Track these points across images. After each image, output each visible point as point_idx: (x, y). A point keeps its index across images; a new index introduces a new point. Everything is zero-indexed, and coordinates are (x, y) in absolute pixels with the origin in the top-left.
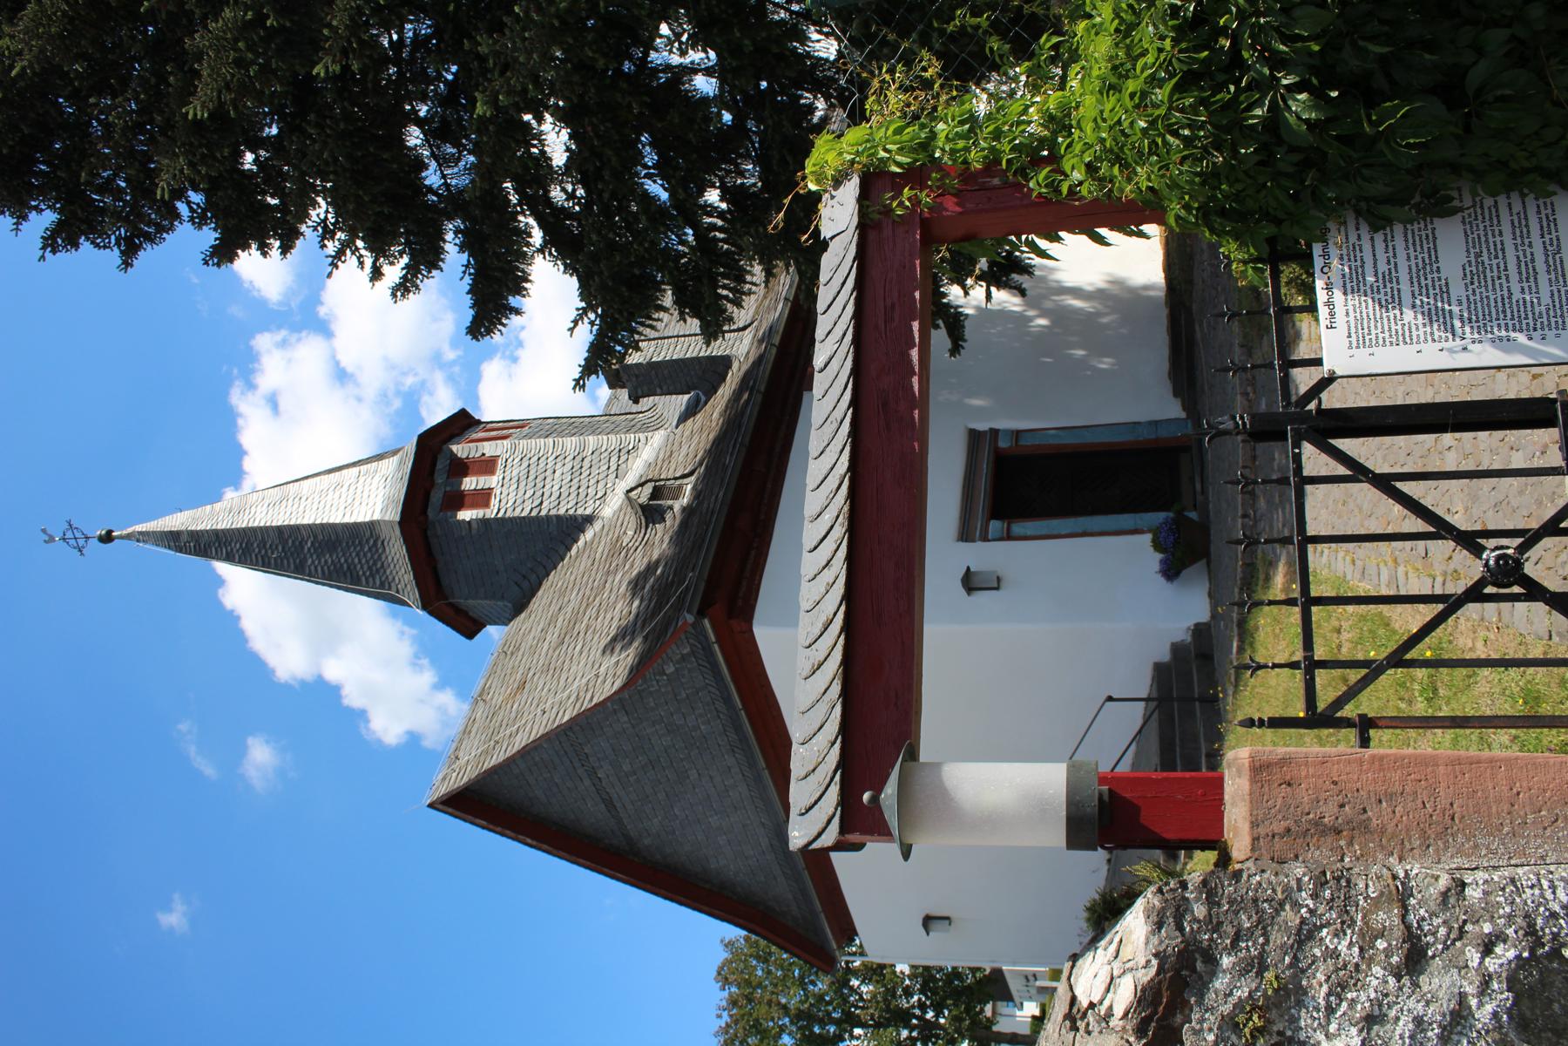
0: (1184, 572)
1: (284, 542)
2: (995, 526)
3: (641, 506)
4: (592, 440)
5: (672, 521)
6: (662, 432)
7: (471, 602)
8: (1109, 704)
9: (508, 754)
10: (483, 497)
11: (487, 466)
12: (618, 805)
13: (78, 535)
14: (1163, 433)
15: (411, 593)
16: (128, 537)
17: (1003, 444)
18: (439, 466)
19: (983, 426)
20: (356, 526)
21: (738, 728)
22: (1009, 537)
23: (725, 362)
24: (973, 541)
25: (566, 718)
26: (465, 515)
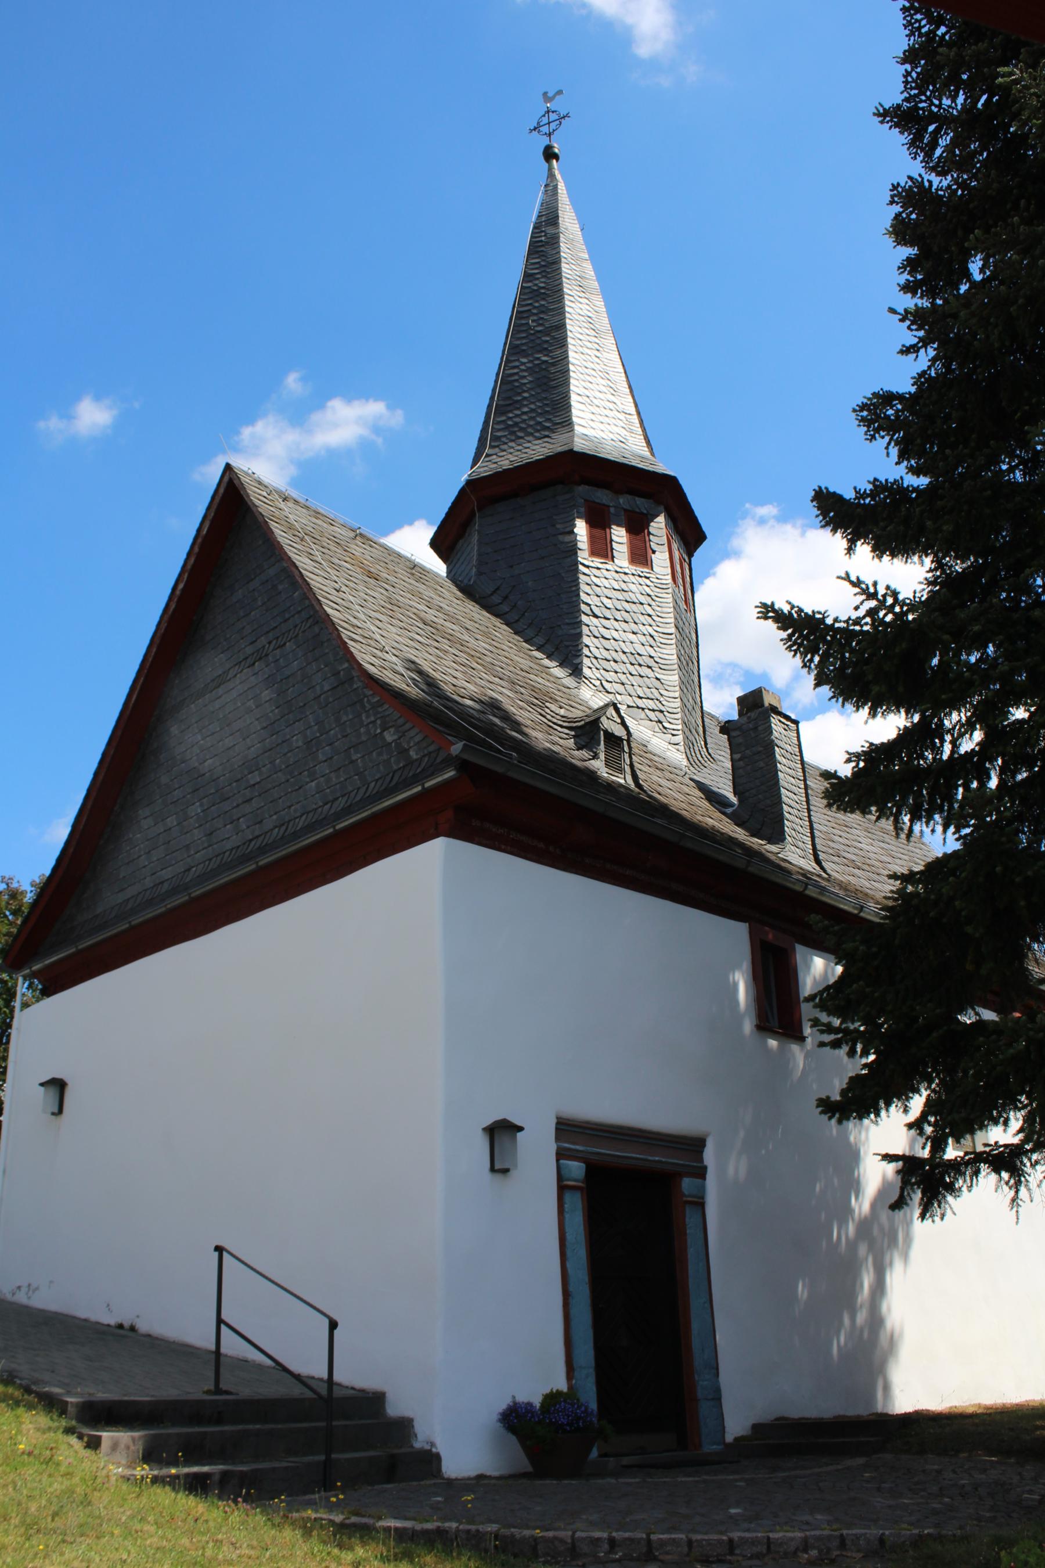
0: (514, 1438)
1: (547, 332)
2: (576, 1169)
3: (597, 721)
4: (673, 678)
5: (579, 757)
6: (685, 762)
7: (475, 538)
8: (327, 1321)
9: (287, 548)
10: (602, 549)
11: (641, 556)
12: (220, 691)
13: (553, 126)
14: (705, 1409)
15: (485, 468)
16: (551, 175)
17: (687, 1184)
18: (639, 501)
19: (709, 1156)
20: (568, 407)
21: (310, 828)
22: (562, 1188)
23: (777, 836)
24: (558, 1139)
25: (329, 611)
26: (581, 528)
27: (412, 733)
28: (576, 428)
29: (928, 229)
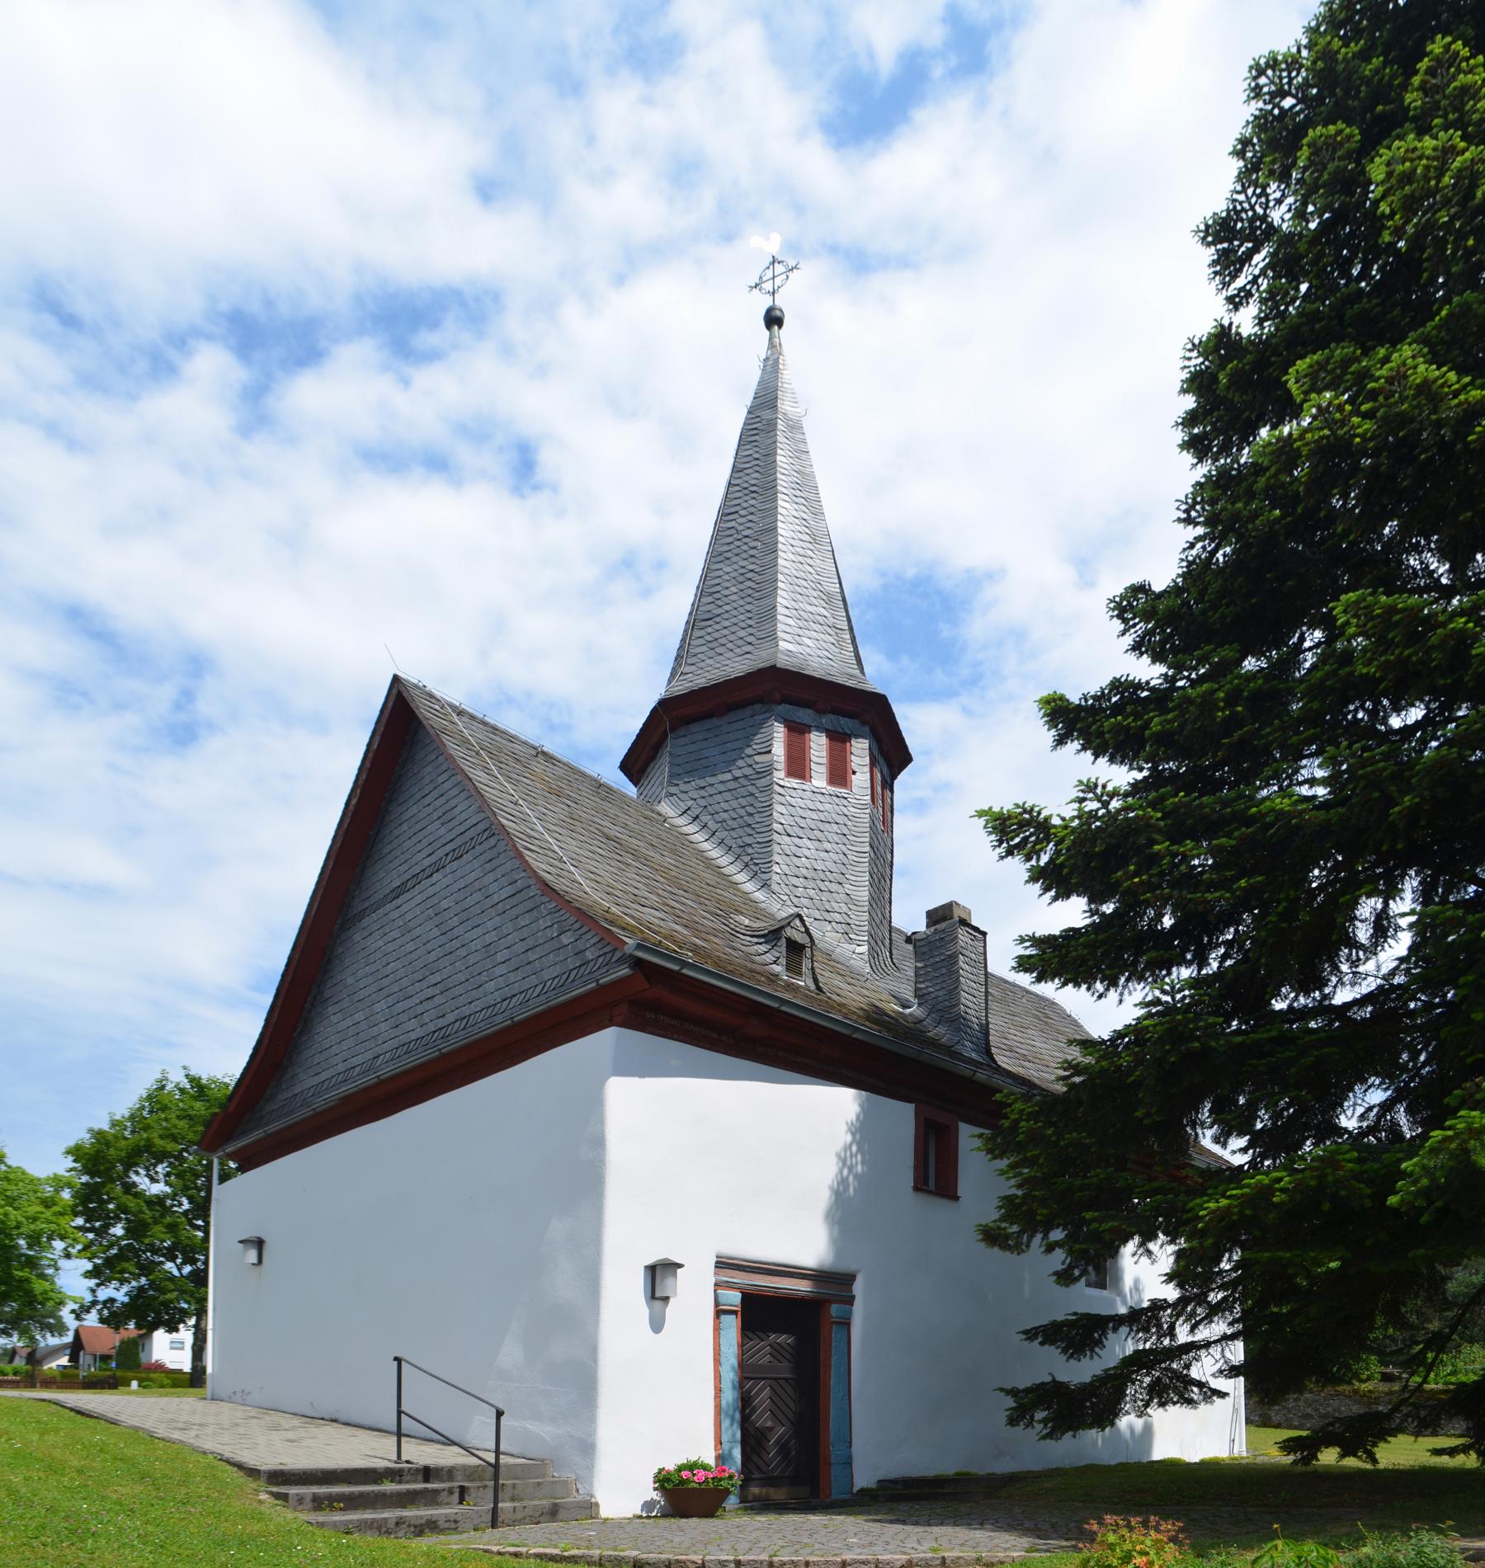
2: (734, 1298)
6: (868, 970)
10: (798, 767)
11: (839, 775)
15: (682, 687)
17: (834, 1309)
18: (843, 721)
19: (858, 1288)
22: (719, 1313)
27: (588, 936)
28: (781, 643)
29: (1229, 390)
